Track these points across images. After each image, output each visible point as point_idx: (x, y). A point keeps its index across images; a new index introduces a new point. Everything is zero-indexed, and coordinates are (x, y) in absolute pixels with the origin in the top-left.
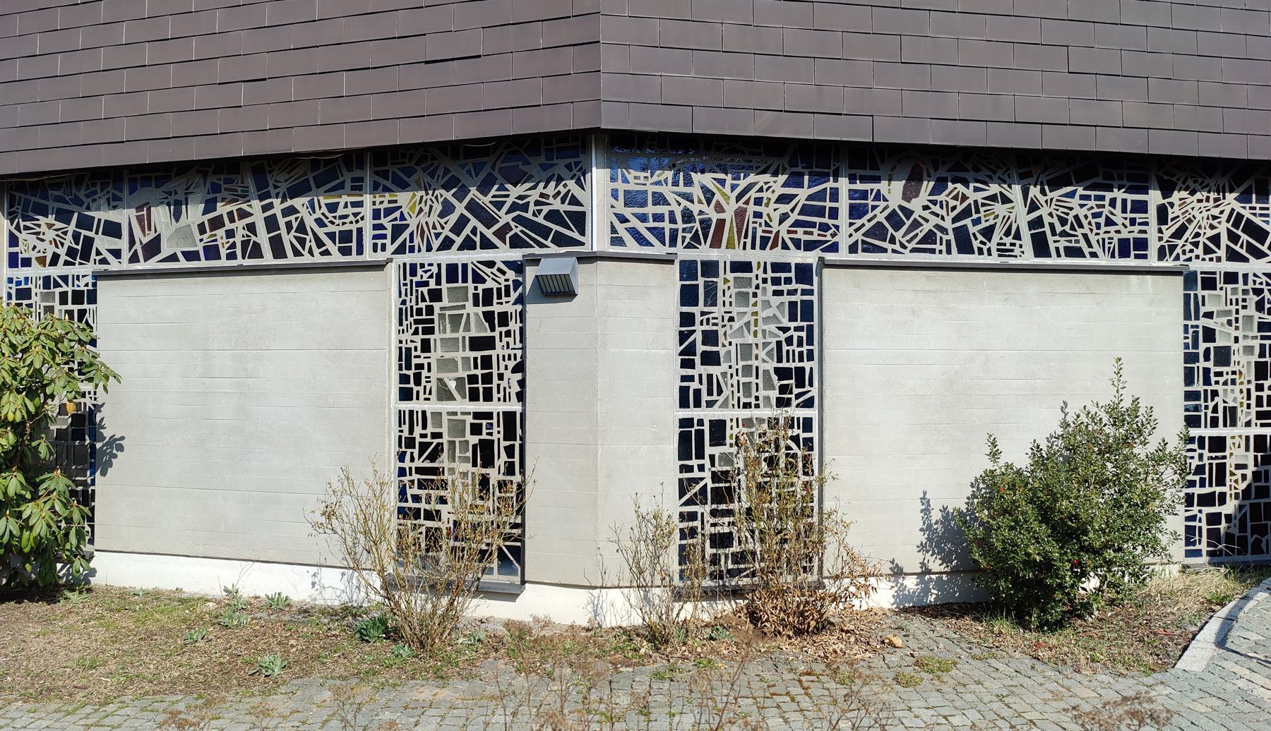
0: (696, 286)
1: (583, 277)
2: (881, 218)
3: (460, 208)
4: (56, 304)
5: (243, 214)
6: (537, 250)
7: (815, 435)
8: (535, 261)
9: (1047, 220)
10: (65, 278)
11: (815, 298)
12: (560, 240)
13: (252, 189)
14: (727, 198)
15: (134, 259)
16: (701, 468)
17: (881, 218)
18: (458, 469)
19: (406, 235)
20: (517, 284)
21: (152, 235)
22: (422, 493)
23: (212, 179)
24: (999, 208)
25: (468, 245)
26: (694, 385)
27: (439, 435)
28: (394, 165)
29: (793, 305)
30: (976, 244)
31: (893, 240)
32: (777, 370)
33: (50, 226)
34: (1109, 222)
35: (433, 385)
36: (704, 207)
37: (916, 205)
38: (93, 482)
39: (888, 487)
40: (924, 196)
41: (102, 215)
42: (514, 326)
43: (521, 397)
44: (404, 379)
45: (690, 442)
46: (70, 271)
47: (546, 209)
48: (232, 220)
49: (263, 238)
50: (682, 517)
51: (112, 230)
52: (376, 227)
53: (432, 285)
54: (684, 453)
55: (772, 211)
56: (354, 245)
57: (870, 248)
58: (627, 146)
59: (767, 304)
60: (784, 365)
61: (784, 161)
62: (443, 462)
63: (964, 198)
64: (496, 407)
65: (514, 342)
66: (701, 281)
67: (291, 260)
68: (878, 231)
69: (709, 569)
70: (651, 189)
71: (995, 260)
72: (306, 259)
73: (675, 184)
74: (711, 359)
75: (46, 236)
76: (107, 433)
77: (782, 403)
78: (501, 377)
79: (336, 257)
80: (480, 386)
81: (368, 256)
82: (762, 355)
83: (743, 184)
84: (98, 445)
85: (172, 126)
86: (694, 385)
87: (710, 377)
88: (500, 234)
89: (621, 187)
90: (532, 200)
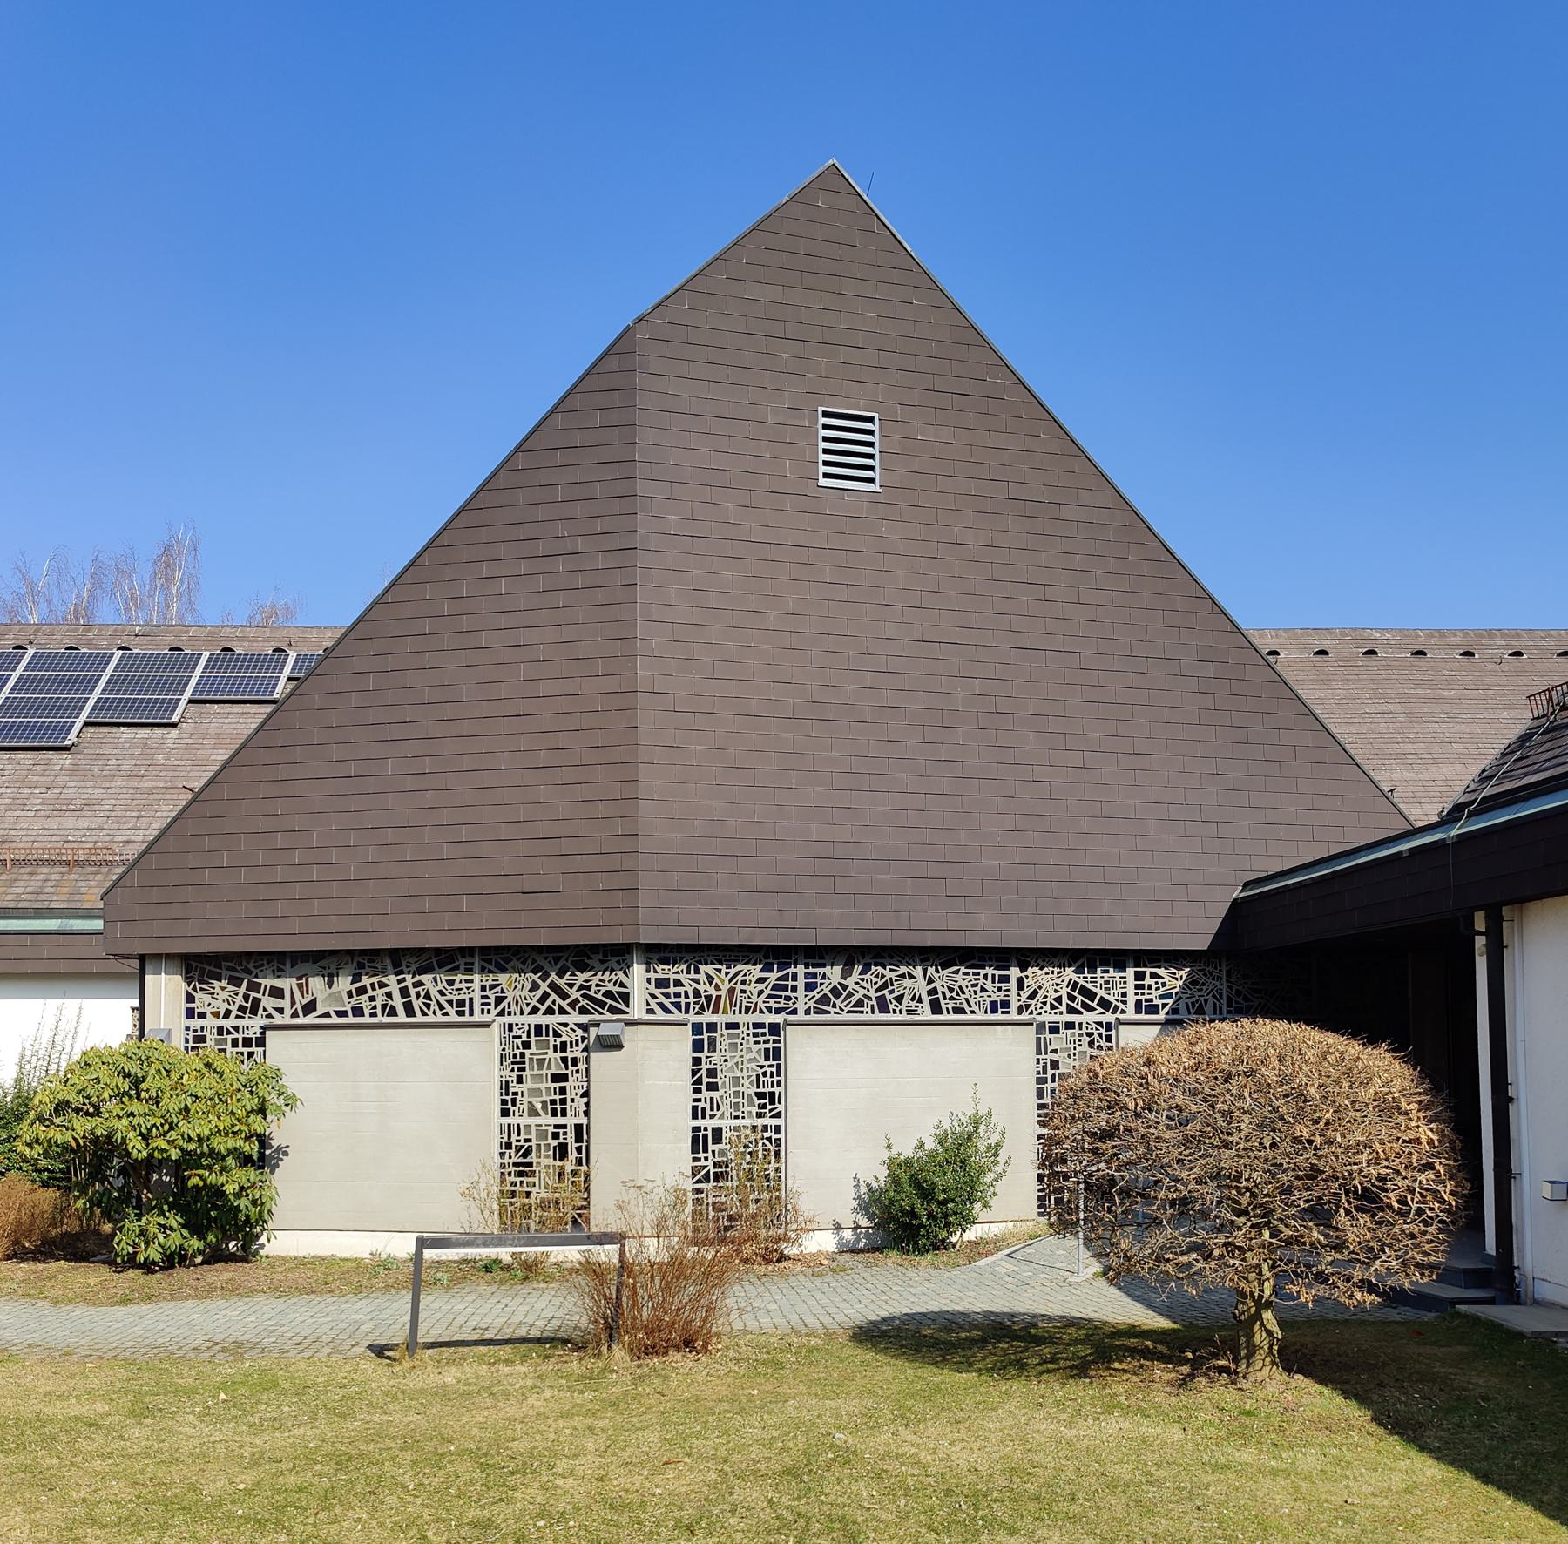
0: (703, 1038)
1: (629, 1036)
2: (827, 991)
3: (544, 987)
4: (229, 1047)
5: (382, 985)
6: (598, 1017)
7: (782, 1136)
8: (597, 1024)
9: (940, 989)
10: (236, 1028)
12: (613, 1010)
13: (390, 967)
15: (295, 1015)
17: (827, 991)
19: (505, 1003)
20: (583, 1039)
22: (518, 1180)
24: (907, 982)
25: (550, 1011)
26: (701, 1105)
28: (497, 958)
29: (767, 1050)
30: (891, 1007)
31: (834, 1006)
33: (223, 989)
34: (983, 990)
35: (525, 1106)
36: (707, 987)
37: (850, 982)
40: (856, 976)
41: (267, 982)
42: (582, 1066)
43: (587, 1113)
44: (504, 1102)
45: (699, 1143)
47: (603, 990)
48: (374, 989)
49: (398, 1002)
51: (277, 993)
53: (524, 1038)
54: (695, 1149)
55: (753, 988)
56: (467, 1009)
57: (818, 1011)
59: (749, 1050)
66: (705, 1036)
67: (419, 1019)
68: (824, 1000)
70: (672, 977)
71: (904, 1017)
72: (430, 1019)
73: (688, 972)
74: (712, 1087)
75: (220, 995)
76: (275, 1143)
77: (759, 1115)
80: (559, 1107)
81: (478, 1017)
82: (747, 1083)
83: (733, 971)
86: (701, 1105)
88: (572, 1005)
89: (653, 976)
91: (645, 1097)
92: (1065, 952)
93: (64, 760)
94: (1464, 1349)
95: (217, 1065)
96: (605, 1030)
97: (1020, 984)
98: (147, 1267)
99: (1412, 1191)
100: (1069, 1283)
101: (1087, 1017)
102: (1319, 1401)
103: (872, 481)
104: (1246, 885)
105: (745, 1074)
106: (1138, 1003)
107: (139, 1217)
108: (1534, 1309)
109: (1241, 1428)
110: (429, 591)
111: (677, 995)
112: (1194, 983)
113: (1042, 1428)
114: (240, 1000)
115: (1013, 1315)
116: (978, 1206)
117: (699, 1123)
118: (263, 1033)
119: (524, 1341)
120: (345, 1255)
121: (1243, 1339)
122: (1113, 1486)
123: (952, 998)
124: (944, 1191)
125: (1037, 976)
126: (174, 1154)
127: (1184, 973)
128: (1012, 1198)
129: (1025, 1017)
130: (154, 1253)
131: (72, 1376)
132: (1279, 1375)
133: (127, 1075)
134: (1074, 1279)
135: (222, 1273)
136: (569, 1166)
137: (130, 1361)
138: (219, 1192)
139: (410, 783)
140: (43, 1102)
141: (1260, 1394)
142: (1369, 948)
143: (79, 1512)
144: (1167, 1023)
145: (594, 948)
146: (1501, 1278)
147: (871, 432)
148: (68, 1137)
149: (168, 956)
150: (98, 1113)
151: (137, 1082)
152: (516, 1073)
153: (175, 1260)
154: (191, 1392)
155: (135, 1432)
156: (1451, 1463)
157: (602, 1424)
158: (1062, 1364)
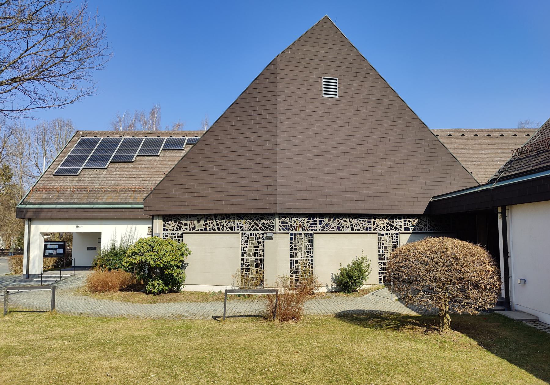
0: (293, 237)
1: (274, 236)
3: (253, 224)
5: (212, 223)
8: (266, 233)
12: (270, 230)
15: (190, 230)
18: (252, 268)
24: (345, 223)
25: (254, 230)
28: (241, 216)
37: (330, 222)
39: (325, 271)
40: (332, 221)
42: (262, 244)
43: (263, 256)
44: (242, 253)
45: (292, 264)
46: (176, 232)
49: (216, 227)
51: (186, 224)
54: (291, 265)
55: (306, 224)
62: (249, 267)
64: (259, 258)
67: (221, 231)
68: (324, 227)
71: (344, 232)
72: (224, 231)
75: (172, 225)
76: (185, 262)
77: (307, 257)
79: (230, 231)
81: (236, 231)
88: (260, 228)
89: (280, 221)
91: (278, 251)
92: (385, 215)
93: (132, 165)
94: (498, 324)
95: (171, 243)
96: (268, 235)
98: (154, 294)
99: (488, 284)
100: (389, 302)
101: (391, 232)
102: (462, 339)
103: (336, 95)
104: (433, 197)
106: (405, 228)
107: (152, 281)
108: (515, 312)
109: (443, 346)
110: (225, 124)
112: (419, 223)
113: (390, 345)
114: (176, 226)
116: (364, 281)
119: (251, 316)
120: (202, 291)
122: (412, 362)
125: (379, 221)
126: (162, 266)
127: (417, 220)
128: (372, 279)
129: (375, 231)
130: (156, 290)
131: (140, 324)
132: (451, 331)
133: (150, 245)
134: (390, 301)
135: (172, 296)
136: (259, 269)
137: (154, 319)
138: (172, 275)
140: (129, 252)
141: (446, 336)
142: (470, 216)
143: (150, 363)
144: (413, 233)
145: (266, 214)
146: (505, 303)
147: (336, 83)
148: (136, 261)
149: (159, 215)
150: (143, 255)
151: (152, 247)
153: (161, 292)
154: (171, 329)
155: (159, 340)
156: (501, 357)
157: (276, 340)
158: (392, 326)
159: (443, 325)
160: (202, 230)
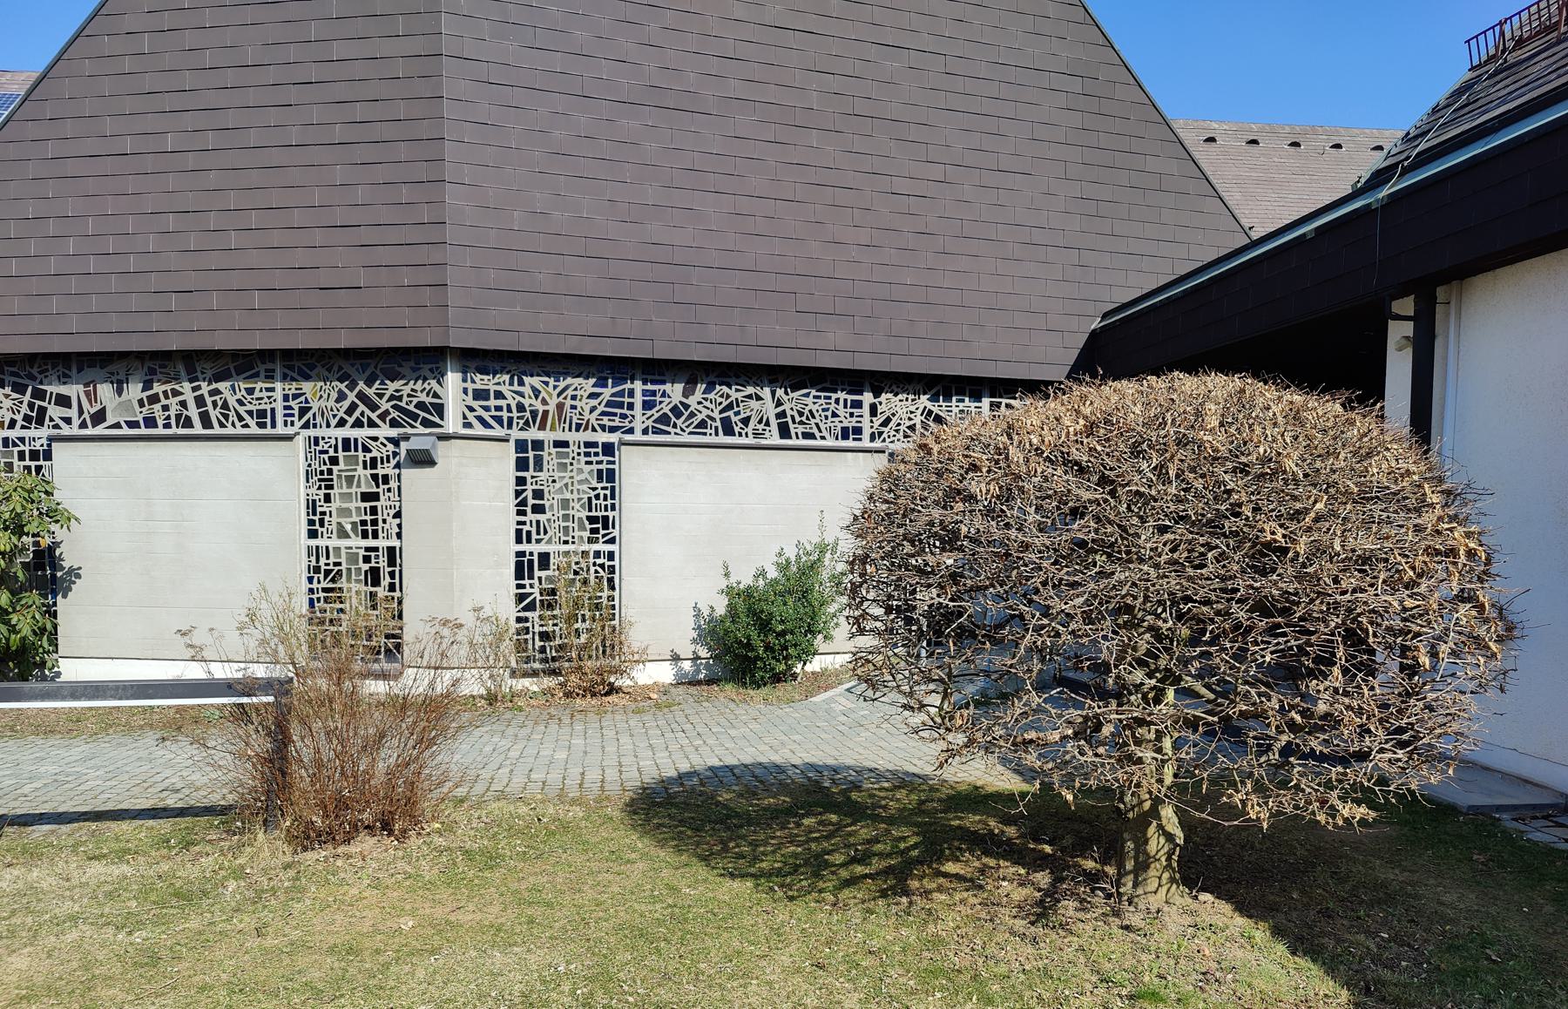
0: (527, 457)
1: (442, 451)
2: (666, 410)
3: (352, 397)
4: (15, 461)
5: (176, 393)
6: (409, 430)
7: (616, 563)
8: (406, 438)
9: (789, 413)
10: (22, 440)
11: (616, 467)
12: (427, 423)
13: (183, 373)
14: (550, 395)
15: (83, 425)
16: (531, 586)
17: (666, 410)
18: (354, 589)
19: (310, 415)
20: (395, 454)
21: (97, 407)
22: (327, 606)
23: (149, 364)
24: (754, 404)
25: (358, 424)
26: (526, 528)
27: (339, 564)
28: (301, 363)
29: (600, 472)
30: (737, 429)
31: (675, 426)
32: (588, 518)
34: (834, 415)
35: (334, 527)
36: (533, 401)
37: (692, 401)
38: (55, 604)
39: (667, 596)
41: (53, 389)
42: (393, 484)
43: (399, 536)
44: (311, 522)
45: (522, 569)
47: (415, 401)
48: (167, 397)
50: (519, 620)
51: (64, 401)
52: (286, 408)
53: (332, 453)
54: (519, 575)
55: (585, 404)
56: (268, 420)
58: (476, 360)
59: (580, 471)
60: (594, 514)
61: (593, 370)
62: (343, 583)
63: (728, 396)
64: (381, 543)
65: (393, 496)
66: (531, 454)
67: (217, 430)
68: (664, 419)
69: (538, 656)
70: (493, 388)
71: (750, 441)
72: (229, 431)
73: (511, 384)
74: (538, 509)
77: (590, 541)
78: (384, 521)
80: (370, 528)
81: (280, 429)
82: (577, 506)
83: (562, 385)
84: (59, 574)
85: (115, 323)
86: (526, 528)
87: (538, 522)
88: (382, 417)
90: (405, 393)
91: (462, 519)
96: (414, 444)
97: (874, 410)
104: (1104, 316)
105: (575, 496)
111: (499, 408)
114: (24, 409)
115: (835, 770)
117: (524, 547)
118: (49, 445)
121: (1130, 845)
123: (801, 423)
124: (782, 622)
125: (890, 402)
129: (877, 444)
132: (1181, 897)
136: (381, 592)
139: (191, 161)
152: (324, 491)
159: (1142, 866)
160: (133, 424)
